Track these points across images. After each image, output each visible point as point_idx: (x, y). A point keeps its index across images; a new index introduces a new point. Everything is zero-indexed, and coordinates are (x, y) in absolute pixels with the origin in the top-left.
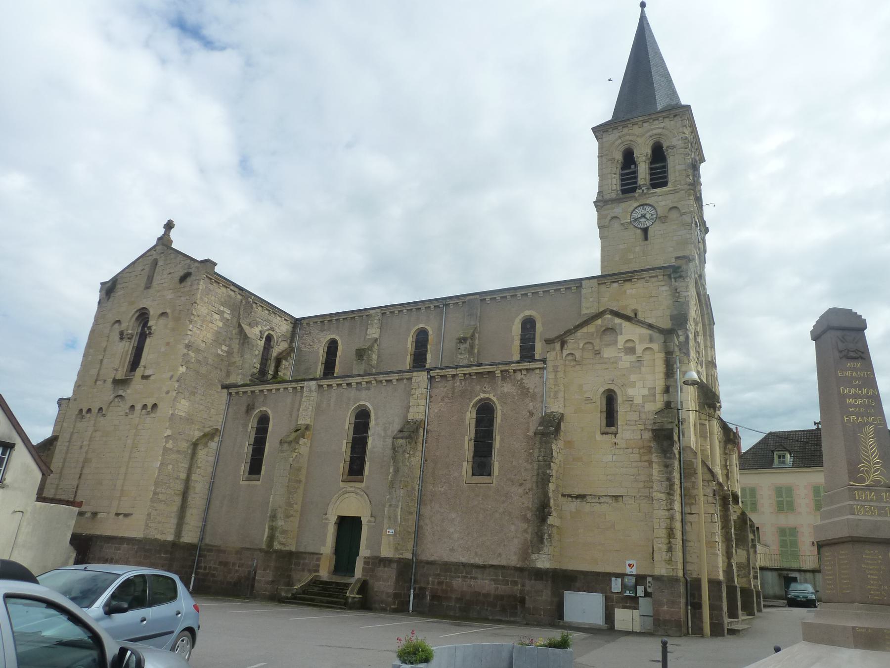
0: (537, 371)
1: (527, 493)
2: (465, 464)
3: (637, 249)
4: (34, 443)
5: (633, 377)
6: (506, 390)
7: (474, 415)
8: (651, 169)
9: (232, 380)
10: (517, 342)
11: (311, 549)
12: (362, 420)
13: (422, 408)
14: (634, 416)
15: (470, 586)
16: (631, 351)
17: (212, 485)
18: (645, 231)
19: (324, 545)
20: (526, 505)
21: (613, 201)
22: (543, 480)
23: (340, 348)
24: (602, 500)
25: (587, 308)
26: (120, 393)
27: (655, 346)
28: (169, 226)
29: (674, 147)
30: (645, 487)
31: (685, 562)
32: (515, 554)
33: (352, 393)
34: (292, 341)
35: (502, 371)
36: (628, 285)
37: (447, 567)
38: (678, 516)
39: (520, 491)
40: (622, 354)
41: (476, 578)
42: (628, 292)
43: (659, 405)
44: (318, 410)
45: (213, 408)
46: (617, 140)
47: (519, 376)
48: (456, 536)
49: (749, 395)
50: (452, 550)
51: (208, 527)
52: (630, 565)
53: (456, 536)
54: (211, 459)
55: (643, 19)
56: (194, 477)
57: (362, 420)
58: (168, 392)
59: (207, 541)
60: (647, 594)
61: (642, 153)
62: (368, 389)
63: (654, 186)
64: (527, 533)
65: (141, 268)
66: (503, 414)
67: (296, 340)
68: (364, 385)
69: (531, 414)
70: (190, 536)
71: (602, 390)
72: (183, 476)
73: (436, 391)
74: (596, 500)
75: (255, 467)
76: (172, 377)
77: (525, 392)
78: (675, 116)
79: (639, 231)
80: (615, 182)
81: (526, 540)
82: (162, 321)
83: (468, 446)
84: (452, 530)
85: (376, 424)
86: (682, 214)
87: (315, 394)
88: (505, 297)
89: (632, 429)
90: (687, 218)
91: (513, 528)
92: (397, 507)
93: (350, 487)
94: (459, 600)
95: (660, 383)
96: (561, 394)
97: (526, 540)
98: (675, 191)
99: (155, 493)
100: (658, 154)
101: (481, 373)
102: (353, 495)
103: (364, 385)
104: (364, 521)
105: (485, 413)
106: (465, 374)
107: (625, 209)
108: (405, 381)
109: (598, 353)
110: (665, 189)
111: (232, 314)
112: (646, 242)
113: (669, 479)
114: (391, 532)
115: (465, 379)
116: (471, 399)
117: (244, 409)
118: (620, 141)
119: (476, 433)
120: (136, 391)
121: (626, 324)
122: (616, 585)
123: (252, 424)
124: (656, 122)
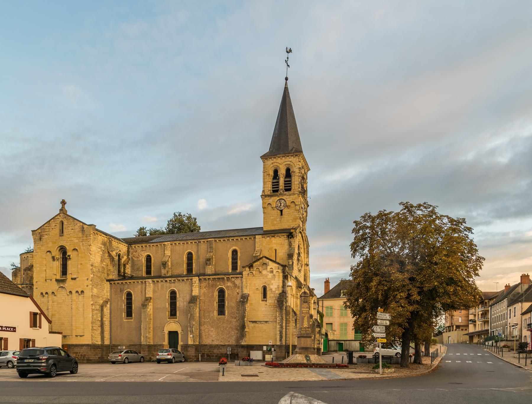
3: (278, 219)
4: (193, 294)
5: (273, 282)
7: (217, 294)
8: (285, 181)
9: (111, 277)
10: (230, 260)
11: (159, 343)
12: (173, 295)
14: (273, 295)
16: (272, 272)
17: (110, 321)
18: (281, 211)
22: (244, 317)
23: (152, 259)
26: (62, 285)
27: (280, 271)
28: (63, 203)
29: (294, 172)
31: (286, 340)
33: (168, 284)
34: (128, 255)
36: (273, 238)
37: (211, 346)
38: (284, 327)
43: (281, 291)
44: (154, 292)
45: (106, 290)
47: (233, 280)
48: (214, 336)
49: (226, 302)
50: (213, 341)
51: (113, 338)
53: (214, 336)
54: (109, 311)
55: (286, 89)
56: (104, 319)
57: (173, 295)
58: (87, 286)
59: (113, 343)
60: (275, 350)
61: (282, 172)
62: (174, 283)
63: (286, 190)
65: (54, 225)
66: (228, 294)
67: (130, 254)
68: (172, 281)
69: (238, 294)
70: (107, 342)
72: (100, 319)
73: (202, 285)
75: (129, 314)
76: (88, 279)
77: (235, 286)
80: (269, 186)
82: (75, 253)
83: (216, 305)
85: (179, 297)
86: (296, 205)
87: (152, 285)
89: (271, 299)
90: (298, 207)
91: (233, 332)
94: (216, 356)
95: (281, 284)
96: (248, 287)
98: (294, 194)
99: (92, 327)
100: (288, 174)
103: (172, 281)
104: (179, 332)
105: (221, 292)
109: (260, 272)
111: (105, 247)
113: (282, 316)
114: (192, 336)
117: (119, 290)
118: (272, 165)
119: (218, 300)
120: (69, 284)
121: (270, 262)
122: (265, 348)
123: (124, 297)
124: (288, 158)
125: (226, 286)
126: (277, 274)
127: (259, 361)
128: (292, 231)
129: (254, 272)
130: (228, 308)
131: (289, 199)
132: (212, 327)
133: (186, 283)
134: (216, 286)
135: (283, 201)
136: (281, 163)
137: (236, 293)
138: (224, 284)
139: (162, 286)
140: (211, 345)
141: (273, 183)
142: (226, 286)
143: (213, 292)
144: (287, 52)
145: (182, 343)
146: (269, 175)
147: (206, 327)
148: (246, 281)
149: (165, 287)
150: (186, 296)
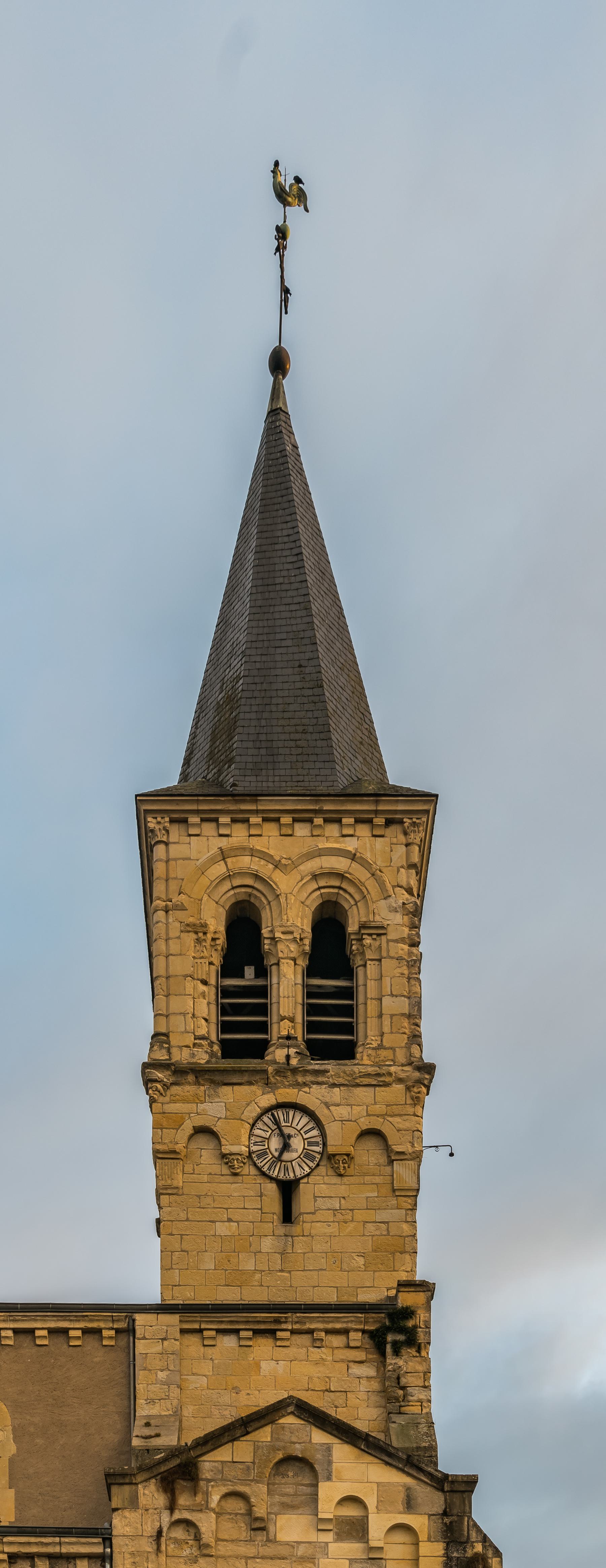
3: (267, 1244)
16: (356, 1529)
18: (288, 1190)
21: (199, 1073)
25: (151, 1401)
27: (419, 1522)
28: (307, 210)
29: (380, 931)
36: (263, 1347)
40: (329, 1537)
42: (266, 1367)
46: (212, 861)
55: (277, 420)
61: (289, 923)
63: (318, 1050)
78: (389, 823)
79: (272, 1189)
80: (199, 1014)
100: (332, 945)
107: (233, 1108)
109: (258, 1526)
110: (348, 1067)
112: (289, 1228)
118: (220, 869)
124: (333, 830)
126: (396, 1550)
128: (406, 1299)
129: (207, 1524)
131: (343, 1112)
135: (301, 1121)
136: (291, 866)
141: (225, 992)
144: (281, 194)
146: (199, 929)
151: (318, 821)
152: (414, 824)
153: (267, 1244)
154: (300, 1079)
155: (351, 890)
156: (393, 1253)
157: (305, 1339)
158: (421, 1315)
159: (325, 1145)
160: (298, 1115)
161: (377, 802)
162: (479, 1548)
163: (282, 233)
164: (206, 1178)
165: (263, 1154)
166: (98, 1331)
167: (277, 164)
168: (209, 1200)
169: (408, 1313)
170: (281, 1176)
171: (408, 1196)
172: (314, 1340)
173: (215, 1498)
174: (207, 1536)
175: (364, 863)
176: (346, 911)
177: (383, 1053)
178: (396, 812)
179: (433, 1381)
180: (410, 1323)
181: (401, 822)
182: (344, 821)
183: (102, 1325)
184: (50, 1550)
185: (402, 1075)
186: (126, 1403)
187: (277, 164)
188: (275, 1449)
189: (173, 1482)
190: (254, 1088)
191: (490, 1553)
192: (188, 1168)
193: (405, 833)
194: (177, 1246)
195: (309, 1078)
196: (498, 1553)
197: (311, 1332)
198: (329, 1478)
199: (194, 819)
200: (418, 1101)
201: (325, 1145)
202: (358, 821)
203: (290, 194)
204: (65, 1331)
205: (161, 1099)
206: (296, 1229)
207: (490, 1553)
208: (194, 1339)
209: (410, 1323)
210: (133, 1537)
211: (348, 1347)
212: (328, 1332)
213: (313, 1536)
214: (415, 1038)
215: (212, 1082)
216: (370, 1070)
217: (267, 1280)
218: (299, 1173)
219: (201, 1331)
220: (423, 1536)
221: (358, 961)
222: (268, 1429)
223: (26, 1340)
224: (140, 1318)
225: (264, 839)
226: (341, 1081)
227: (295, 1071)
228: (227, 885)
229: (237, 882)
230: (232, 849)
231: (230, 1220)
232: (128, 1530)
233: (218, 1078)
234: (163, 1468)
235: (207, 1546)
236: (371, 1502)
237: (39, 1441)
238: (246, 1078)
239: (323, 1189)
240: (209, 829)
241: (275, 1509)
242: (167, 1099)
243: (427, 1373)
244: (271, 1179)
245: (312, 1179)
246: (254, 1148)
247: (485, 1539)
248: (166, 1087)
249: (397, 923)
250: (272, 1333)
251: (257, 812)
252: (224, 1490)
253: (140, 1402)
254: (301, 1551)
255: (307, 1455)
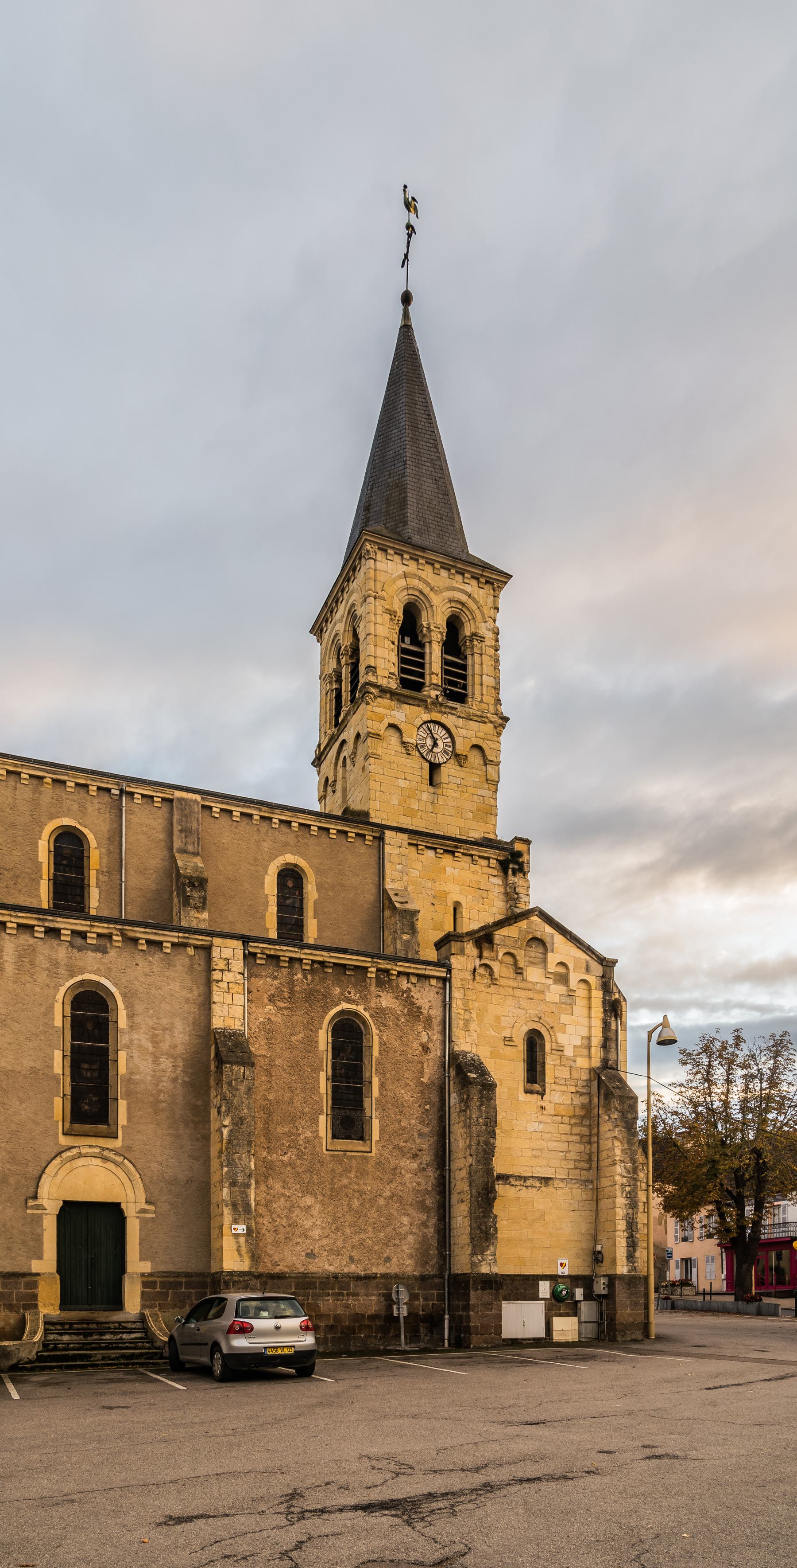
0: (433, 982)
1: (424, 1169)
2: (322, 1119)
4: (217, 1023)
5: (564, 1018)
6: (384, 1004)
12: (91, 1015)
13: (238, 1011)
14: (564, 1073)
15: (347, 1306)
16: (563, 979)
18: (434, 768)
19: (40, 1258)
20: (422, 1187)
24: (528, 1183)
25: (393, 881)
29: (482, 639)
30: (576, 1168)
32: (411, 1256)
35: (378, 970)
36: (448, 858)
39: (414, 1165)
40: (550, 981)
41: (356, 1295)
42: (449, 870)
43: (596, 1062)
47: (404, 984)
48: (316, 1233)
49: (376, 1081)
52: (561, 1264)
53: (316, 1233)
55: (406, 331)
57: (91, 1015)
62: (101, 949)
64: (427, 1227)
66: (382, 1044)
68: (92, 940)
69: (426, 1049)
71: (525, 1029)
74: (522, 1183)
77: (415, 1013)
78: (487, 582)
79: (426, 766)
81: (425, 1236)
84: (308, 1224)
85: (133, 1027)
88: (250, 816)
91: (405, 1220)
92: (248, 1186)
93: (85, 1144)
96: (473, 1026)
97: (425, 1236)
101: (344, 966)
102: (98, 1161)
104: (131, 1211)
105: (349, 1036)
106: (313, 962)
108: (191, 951)
109: (519, 971)
114: (241, 1228)
115: (312, 971)
116: (326, 1009)
118: (402, 583)
122: (545, 1289)
124: (459, 578)
125: (373, 1005)
127: (536, 1343)
128: (518, 847)
130: (382, 1106)
131: (463, 732)
132: (307, 1190)
133: (169, 963)
134: (327, 1002)
135: (440, 733)
137: (416, 1045)
138: (365, 999)
139: (25, 956)
140: (304, 1275)
142: (373, 1005)
143: (312, 1029)
144: (408, 205)
145: (146, 1267)
147: (278, 1187)
148: (465, 1000)
149: (42, 960)
150: (170, 1029)
151: (453, 571)
152: (499, 587)
153: (425, 796)
154: (443, 710)
155: (467, 613)
156: (486, 814)
157: (468, 859)
158: (525, 855)
159: (454, 747)
160: (441, 729)
161: (483, 571)
162: (617, 996)
163: (409, 226)
164: (393, 753)
165: (423, 746)
166: (364, 836)
167: (405, 187)
168: (395, 765)
169: (519, 854)
170: (432, 760)
171: (493, 784)
172: (473, 860)
173: (500, 955)
174: (496, 975)
175: (474, 600)
176: (463, 623)
177: (483, 706)
178: (491, 578)
179: (530, 892)
180: (521, 860)
181: (492, 584)
182: (466, 575)
183: (366, 833)
184: (420, 972)
185: (493, 720)
186: (377, 879)
187: (405, 187)
188: (529, 933)
189: (481, 944)
190: (420, 709)
191: (622, 999)
192: (385, 745)
193: (494, 590)
194: (378, 788)
195: (448, 710)
196: (625, 1000)
197: (472, 856)
198: (553, 951)
199: (390, 551)
200: (499, 734)
201: (454, 747)
202: (473, 577)
203: (410, 205)
204: (346, 833)
205: (372, 703)
206: (439, 791)
207: (622, 999)
208: (413, 849)
209: (521, 860)
210: (462, 970)
211: (489, 866)
212: (480, 857)
213: (544, 980)
214: (498, 701)
215: (399, 700)
216: (478, 713)
217: (424, 816)
218: (441, 761)
219: (417, 845)
220: (593, 987)
221: (469, 652)
222: (525, 921)
223: (324, 834)
224: (388, 833)
225: (425, 573)
226: (463, 715)
227: (441, 705)
228: (405, 592)
229: (411, 592)
230: (409, 574)
231: (405, 779)
232: (459, 966)
233: (402, 699)
234: (477, 936)
235: (496, 979)
236: (571, 966)
237: (331, 893)
238: (416, 703)
239: (452, 772)
240: (397, 558)
241: (527, 964)
242: (375, 704)
243: (528, 888)
244: (427, 760)
245: (447, 765)
246: (419, 742)
247: (619, 992)
248: (376, 697)
249: (489, 635)
250: (452, 853)
251: (423, 557)
252: (505, 951)
253: (387, 880)
254: (538, 987)
255: (543, 938)
